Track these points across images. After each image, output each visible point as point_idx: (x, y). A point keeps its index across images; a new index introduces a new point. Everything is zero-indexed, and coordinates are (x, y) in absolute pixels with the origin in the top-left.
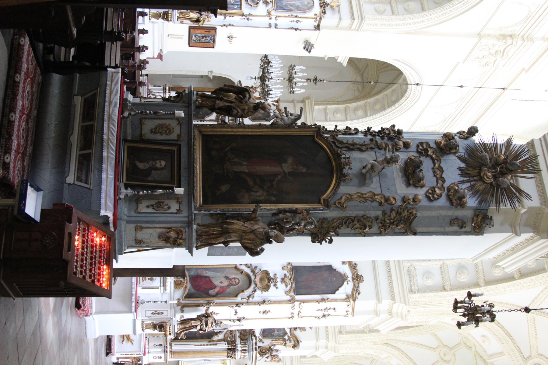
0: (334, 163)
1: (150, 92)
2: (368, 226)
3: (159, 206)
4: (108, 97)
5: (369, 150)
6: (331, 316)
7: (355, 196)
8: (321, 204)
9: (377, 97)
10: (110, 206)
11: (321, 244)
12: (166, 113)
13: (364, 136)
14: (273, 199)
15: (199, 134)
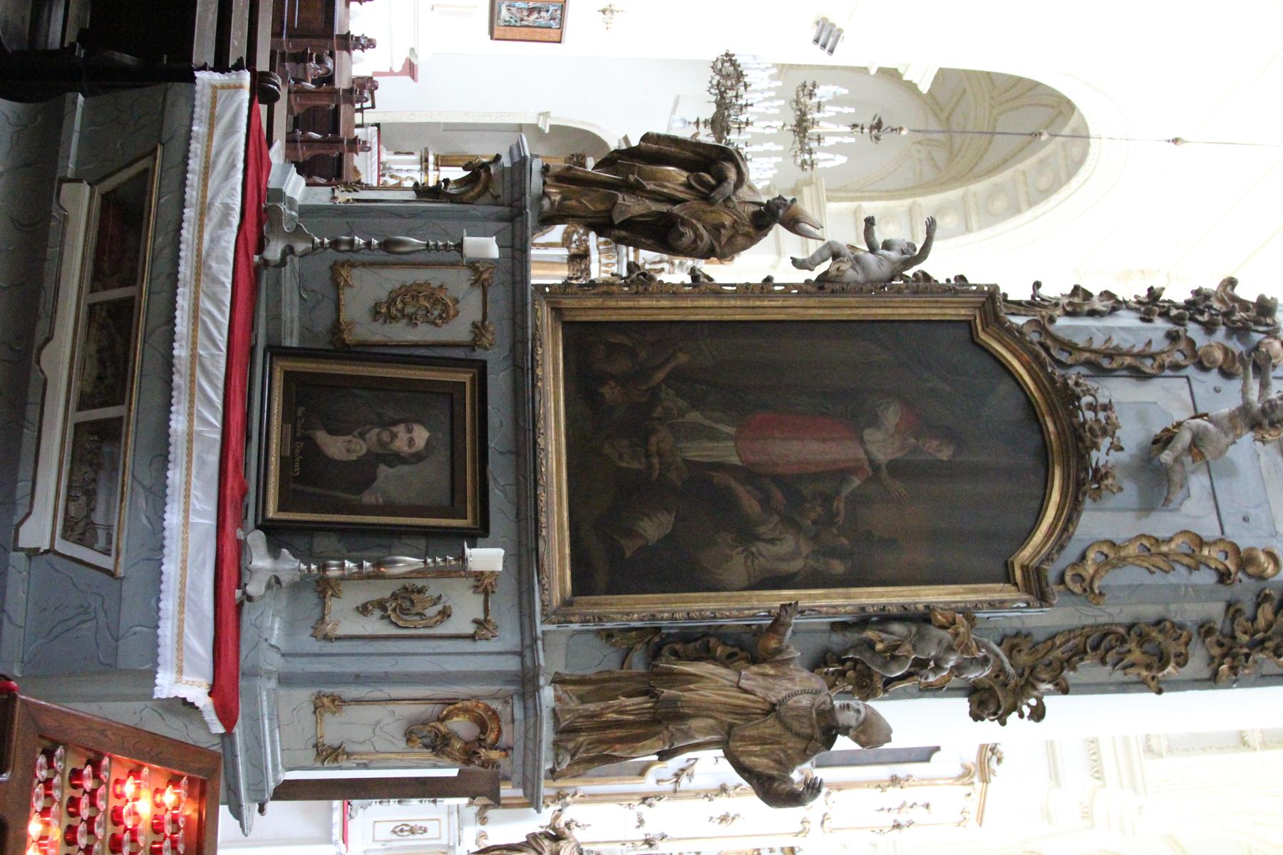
0: (1051, 427)
1: (384, 168)
2: (1172, 656)
3: (407, 604)
4: (196, 184)
5: (1168, 372)
6: (918, 825)
8: (1016, 584)
9: (997, 179)
10: (194, 653)
11: (1003, 723)
12: (428, 245)
13: (1143, 320)
14: (838, 567)
15: (555, 319)
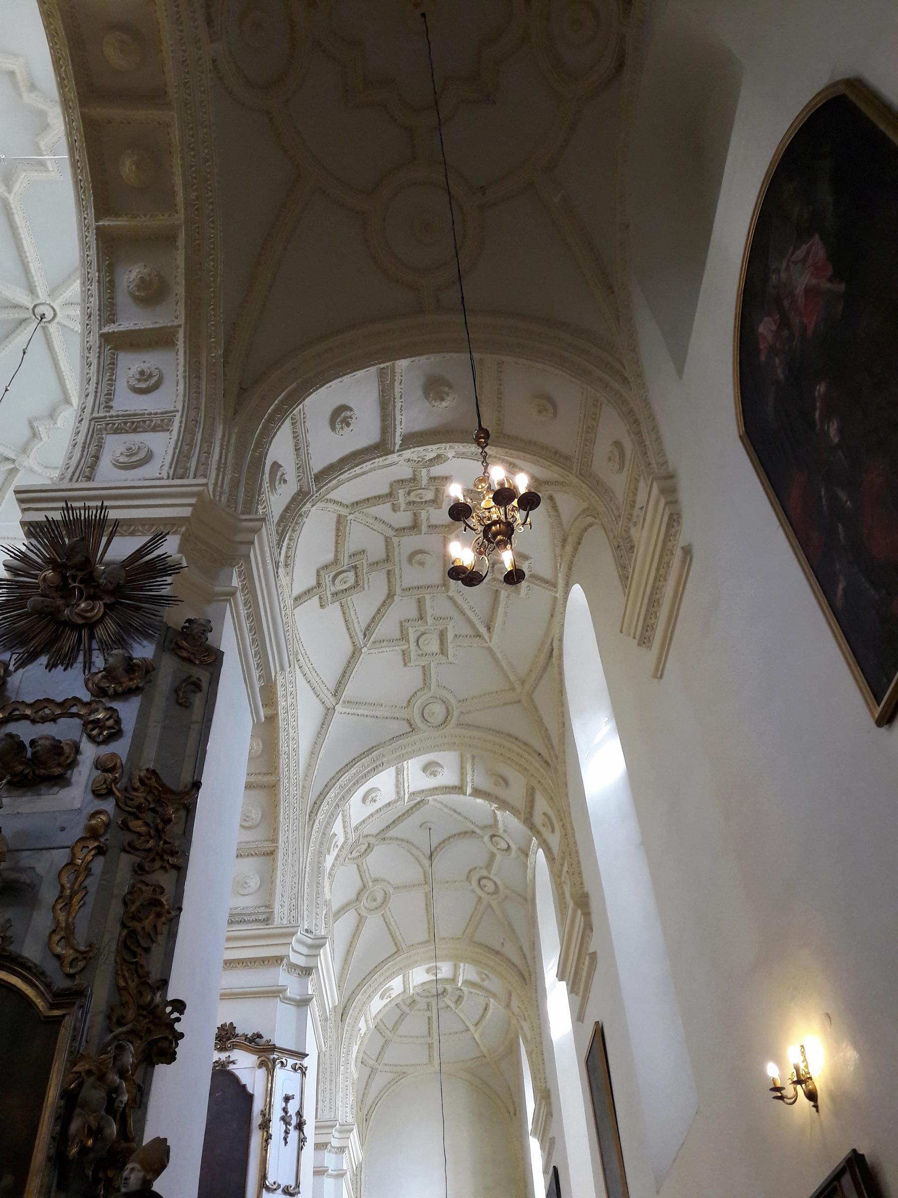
7: (62, 917)
8: (64, 1016)
11: (182, 1035)
